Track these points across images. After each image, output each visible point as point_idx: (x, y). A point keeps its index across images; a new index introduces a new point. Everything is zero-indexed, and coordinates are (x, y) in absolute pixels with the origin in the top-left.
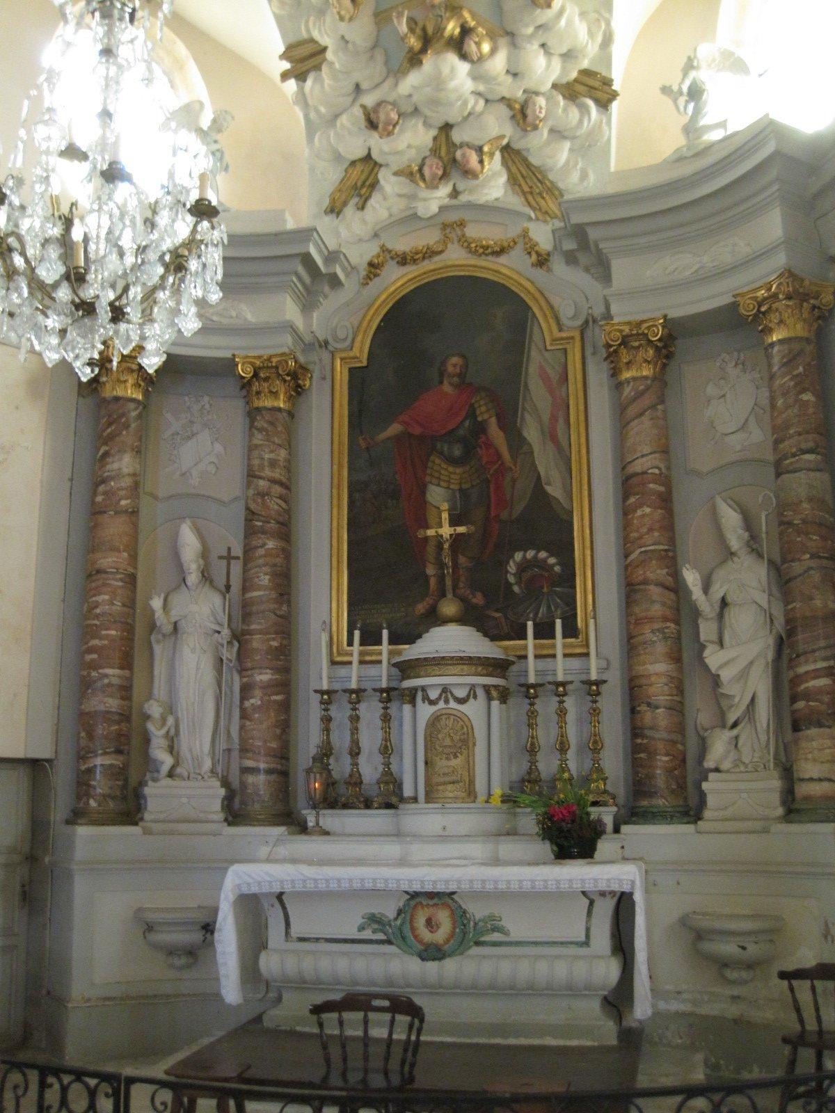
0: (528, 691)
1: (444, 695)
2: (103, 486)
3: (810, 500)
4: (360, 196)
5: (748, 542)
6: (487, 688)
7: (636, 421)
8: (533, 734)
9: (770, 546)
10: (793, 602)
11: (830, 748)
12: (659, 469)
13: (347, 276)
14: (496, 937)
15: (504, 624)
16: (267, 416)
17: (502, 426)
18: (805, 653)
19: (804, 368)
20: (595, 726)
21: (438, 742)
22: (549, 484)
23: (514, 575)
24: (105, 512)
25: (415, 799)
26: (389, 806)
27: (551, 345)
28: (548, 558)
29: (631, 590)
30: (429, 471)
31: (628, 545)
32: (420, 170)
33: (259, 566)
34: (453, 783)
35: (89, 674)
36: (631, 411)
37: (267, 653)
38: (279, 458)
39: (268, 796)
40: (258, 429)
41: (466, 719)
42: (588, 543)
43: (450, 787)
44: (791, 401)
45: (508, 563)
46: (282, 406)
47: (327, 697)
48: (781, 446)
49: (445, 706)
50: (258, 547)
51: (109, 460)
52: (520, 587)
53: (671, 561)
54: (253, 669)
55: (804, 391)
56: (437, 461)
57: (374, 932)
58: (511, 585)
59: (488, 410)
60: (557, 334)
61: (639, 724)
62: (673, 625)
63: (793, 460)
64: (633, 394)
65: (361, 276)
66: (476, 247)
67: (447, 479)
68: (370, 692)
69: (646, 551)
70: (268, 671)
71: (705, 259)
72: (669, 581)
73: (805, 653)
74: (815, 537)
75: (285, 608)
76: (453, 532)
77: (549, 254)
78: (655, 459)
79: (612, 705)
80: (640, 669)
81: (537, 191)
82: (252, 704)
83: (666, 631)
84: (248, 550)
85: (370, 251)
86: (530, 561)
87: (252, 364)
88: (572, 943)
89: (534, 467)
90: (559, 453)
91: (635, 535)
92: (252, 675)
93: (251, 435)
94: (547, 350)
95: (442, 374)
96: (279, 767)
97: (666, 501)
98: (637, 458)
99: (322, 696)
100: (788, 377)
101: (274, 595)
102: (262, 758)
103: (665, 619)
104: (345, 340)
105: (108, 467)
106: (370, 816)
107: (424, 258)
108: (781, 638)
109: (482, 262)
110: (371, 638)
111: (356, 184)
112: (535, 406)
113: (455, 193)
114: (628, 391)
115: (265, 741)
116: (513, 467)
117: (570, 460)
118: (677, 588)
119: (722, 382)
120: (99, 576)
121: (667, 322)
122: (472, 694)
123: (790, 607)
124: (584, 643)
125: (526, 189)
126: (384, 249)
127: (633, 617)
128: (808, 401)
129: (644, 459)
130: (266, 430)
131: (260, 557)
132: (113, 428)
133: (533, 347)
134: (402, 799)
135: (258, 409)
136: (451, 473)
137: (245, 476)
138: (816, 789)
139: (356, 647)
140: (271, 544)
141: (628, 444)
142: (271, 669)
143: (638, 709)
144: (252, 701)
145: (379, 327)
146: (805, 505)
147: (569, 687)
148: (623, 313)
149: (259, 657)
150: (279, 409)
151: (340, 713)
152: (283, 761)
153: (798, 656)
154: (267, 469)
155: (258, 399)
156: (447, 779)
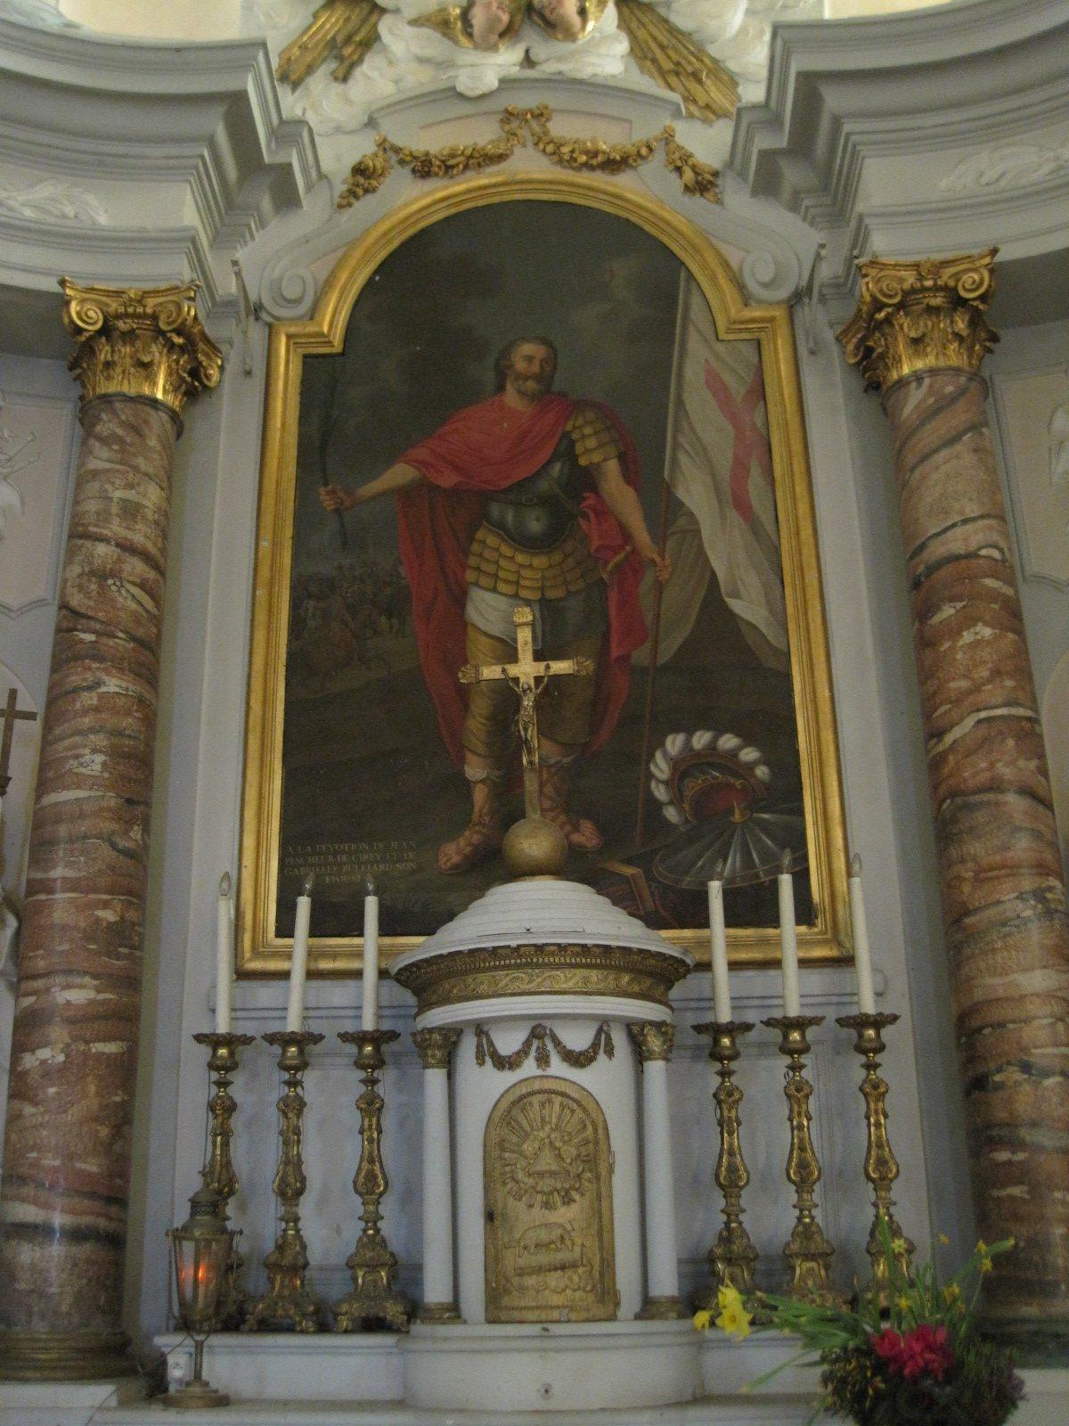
0: (716, 1042)
1: (535, 1043)
4: (341, 59)
6: (636, 1032)
7: (944, 453)
8: (731, 1145)
12: (1001, 551)
13: (309, 188)
15: (646, 893)
16: (126, 412)
17: (631, 475)
21: (522, 1163)
25: (453, 1311)
26: (372, 1325)
27: (729, 330)
30: (472, 561)
32: (465, 16)
33: (79, 732)
34: (563, 1268)
37: (89, 938)
38: (145, 502)
39: (69, 1299)
41: (591, 1106)
42: (826, 717)
43: (554, 1279)
45: (651, 756)
46: (160, 396)
49: (539, 1072)
50: (84, 689)
52: (681, 810)
54: (47, 974)
56: (492, 540)
59: (600, 446)
60: (735, 311)
64: (931, 401)
65: (337, 193)
66: (573, 151)
67: (512, 577)
68: (331, 1041)
70: (87, 980)
75: (136, 833)
76: (542, 673)
77: (716, 174)
78: (991, 528)
80: (990, 984)
81: (690, 69)
82: (43, 1062)
83: (1049, 895)
84: (58, 700)
85: (362, 148)
86: (698, 754)
87: (102, 306)
89: (701, 553)
92: (47, 990)
93: (85, 451)
95: (502, 375)
96: (102, 1223)
98: (954, 525)
99: (215, 1051)
101: (111, 800)
102: (59, 1201)
104: (297, 302)
106: (334, 1352)
107: (466, 167)
109: (585, 178)
111: (334, 38)
112: (699, 439)
113: (528, 61)
114: (914, 400)
115: (71, 1157)
116: (658, 559)
117: (777, 550)
122: (601, 1045)
124: (829, 936)
125: (667, 65)
126: (384, 146)
127: (970, 865)
129: (969, 527)
131: (86, 711)
133: (691, 329)
134: (415, 1310)
135: (107, 399)
136: (521, 566)
137: (65, 537)
139: (301, 939)
140: (112, 685)
142: (95, 976)
143: (997, 1078)
144: (44, 1053)
145: (370, 283)
149: (65, 947)
150: (154, 403)
152: (114, 1210)
154: (116, 521)
155: (109, 378)
156: (544, 1258)
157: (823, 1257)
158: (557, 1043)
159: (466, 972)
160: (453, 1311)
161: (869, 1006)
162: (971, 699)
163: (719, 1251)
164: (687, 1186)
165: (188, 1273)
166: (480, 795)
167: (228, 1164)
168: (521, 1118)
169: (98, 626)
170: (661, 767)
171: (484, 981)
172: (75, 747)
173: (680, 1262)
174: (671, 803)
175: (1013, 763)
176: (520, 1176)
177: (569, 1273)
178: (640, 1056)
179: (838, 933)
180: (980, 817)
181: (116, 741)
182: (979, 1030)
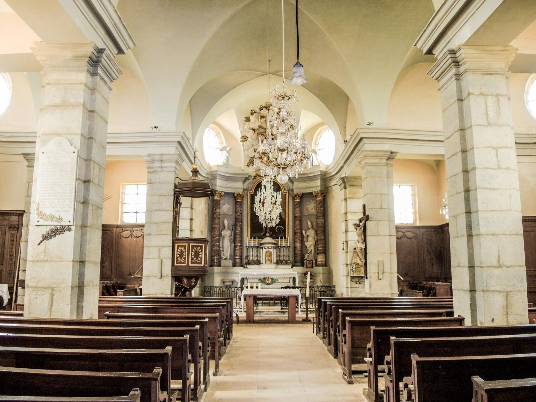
3: (321, 223)
6: (274, 247)
14: (277, 282)
25: (263, 263)
29: (295, 234)
36: (296, 206)
47: (248, 248)
53: (301, 229)
71: (309, 184)
72: (301, 232)
79: (291, 250)
97: (300, 220)
110: (255, 238)
114: (296, 203)
118: (302, 233)
122: (272, 248)
139: (253, 240)
148: (296, 191)
160: (263, 263)
161: (289, 245)
164: (277, 256)
166: (264, 230)
170: (276, 228)
178: (274, 248)
179: (287, 240)
181: (182, 162)
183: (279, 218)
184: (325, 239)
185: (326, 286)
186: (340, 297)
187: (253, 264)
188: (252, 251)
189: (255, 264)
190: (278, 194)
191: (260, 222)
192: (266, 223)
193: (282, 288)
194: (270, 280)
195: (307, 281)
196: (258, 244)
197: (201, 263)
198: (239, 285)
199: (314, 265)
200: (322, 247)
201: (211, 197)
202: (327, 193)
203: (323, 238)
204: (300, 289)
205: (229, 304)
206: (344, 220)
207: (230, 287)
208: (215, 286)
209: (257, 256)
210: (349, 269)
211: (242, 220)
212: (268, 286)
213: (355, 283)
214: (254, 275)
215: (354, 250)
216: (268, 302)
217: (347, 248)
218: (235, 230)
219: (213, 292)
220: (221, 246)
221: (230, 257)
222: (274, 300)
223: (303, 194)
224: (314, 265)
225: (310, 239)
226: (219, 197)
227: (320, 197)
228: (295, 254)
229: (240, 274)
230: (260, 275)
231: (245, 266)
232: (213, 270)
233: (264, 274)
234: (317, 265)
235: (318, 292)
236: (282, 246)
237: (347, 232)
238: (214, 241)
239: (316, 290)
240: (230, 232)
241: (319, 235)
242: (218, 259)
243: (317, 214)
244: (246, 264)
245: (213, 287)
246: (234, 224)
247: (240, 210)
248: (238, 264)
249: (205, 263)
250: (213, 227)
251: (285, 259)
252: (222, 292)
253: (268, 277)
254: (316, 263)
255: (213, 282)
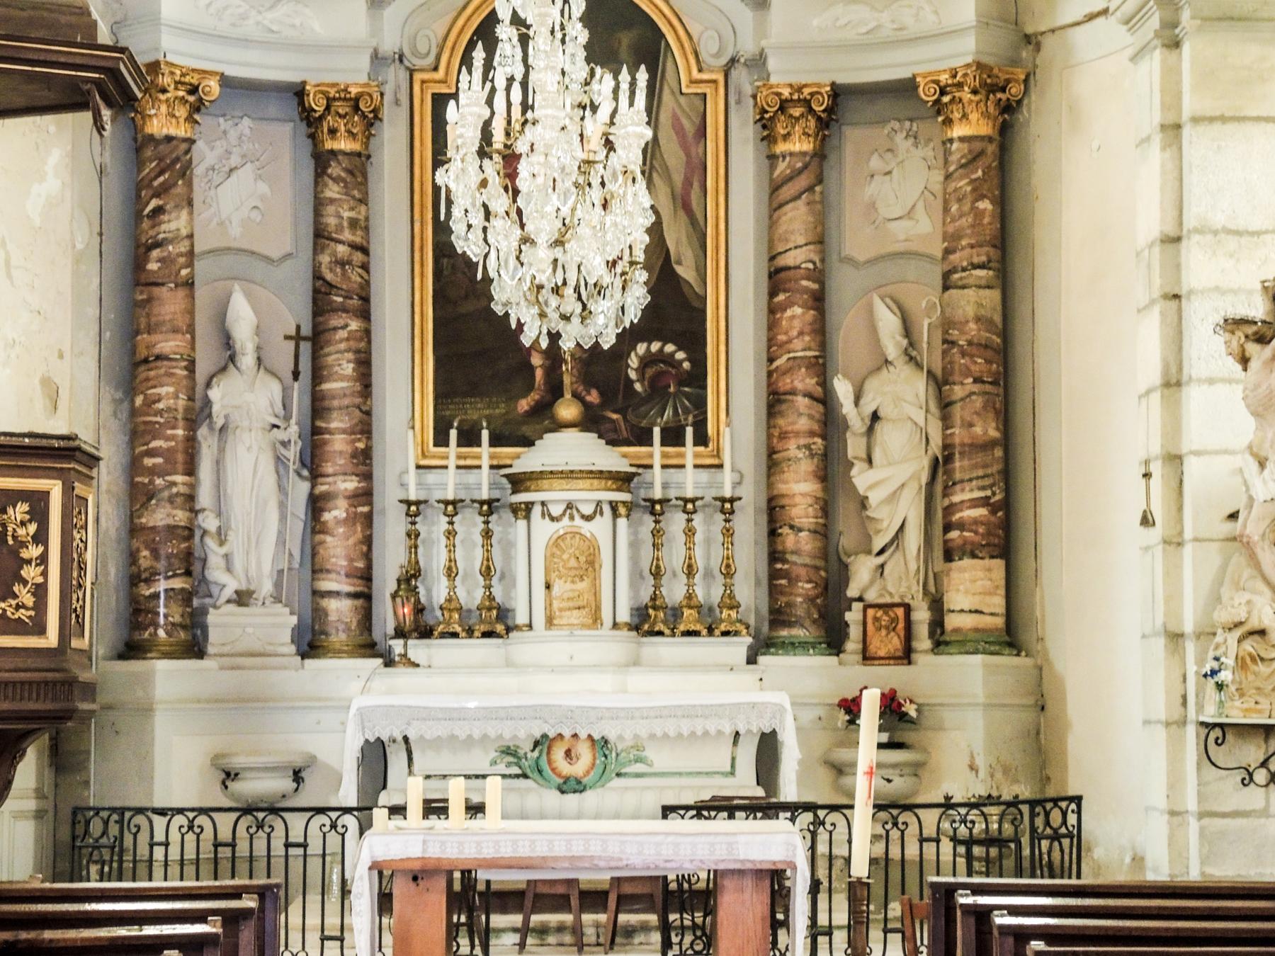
0: (653, 507)
1: (569, 511)
2: (158, 250)
3: (978, 319)
5: (906, 349)
6: (614, 506)
7: (790, 206)
9: (932, 356)
10: (952, 427)
11: (982, 579)
12: (814, 263)
14: (639, 768)
18: (962, 481)
19: (983, 171)
20: (728, 549)
22: (679, 263)
23: (636, 370)
24: (163, 284)
28: (676, 352)
29: (775, 401)
31: (774, 348)
34: (579, 608)
35: (152, 482)
36: (787, 192)
40: (334, 179)
44: (966, 208)
45: (629, 355)
47: (414, 508)
48: (952, 257)
51: (165, 217)
52: (643, 385)
53: (822, 367)
55: (982, 197)
57: (509, 765)
58: (632, 382)
60: (696, 75)
61: (780, 548)
62: (819, 441)
63: (964, 274)
64: (788, 171)
69: (794, 358)
70: (354, 478)
71: (885, 17)
73: (962, 481)
74: (979, 360)
79: (748, 525)
80: (782, 488)
82: (335, 517)
86: (654, 355)
88: (718, 773)
90: (692, 224)
91: (782, 338)
92: (335, 482)
94: (681, 93)
97: (819, 301)
98: (790, 249)
100: (967, 180)
103: (812, 434)
105: (164, 227)
108: (937, 459)
110: (469, 438)
114: (782, 167)
117: (705, 235)
118: (826, 400)
119: (889, 155)
120: (159, 363)
121: (833, 84)
122: (598, 510)
123: (949, 432)
124: (715, 453)
128: (985, 209)
129: (798, 250)
130: (344, 180)
131: (341, 341)
132: (167, 176)
138: (967, 622)
141: (780, 231)
143: (780, 531)
144: (335, 513)
146: (972, 325)
147: (698, 503)
151: (434, 526)
153: (954, 484)
157: (699, 607)
158: (578, 510)
159: (537, 479)
160: (530, 626)
162: (787, 346)
163: (650, 604)
164: (636, 576)
165: (400, 612)
166: (539, 373)
167: (417, 562)
168: (562, 544)
169: (343, 293)
170: (634, 362)
171: (545, 483)
172: (339, 359)
173: (632, 609)
174: (638, 380)
175: (803, 380)
176: (561, 569)
177: (582, 610)
178: (615, 514)
180: (784, 407)
181: (358, 356)
182: (775, 508)
183: (642, 276)
184: (1007, 440)
185: (1007, 797)
186: (1121, 876)
187: (455, 635)
188: (451, 534)
189: (470, 633)
190: (625, 86)
191: (499, 310)
192: (542, 315)
193: (667, 811)
194: (585, 754)
195: (853, 765)
196: (493, 486)
197: (41, 630)
198: (348, 795)
199: (923, 642)
200: (985, 502)
201: (106, 114)
202: (1026, 81)
203: (994, 433)
204: (807, 817)
205: (247, 935)
206: (1156, 294)
207: (274, 811)
208: (158, 803)
209: (487, 572)
210: (1192, 669)
211: (366, 299)
212: (571, 798)
213: (1239, 775)
214: (458, 715)
215: (1228, 528)
216: (568, 918)
217: (1180, 509)
218: (318, 376)
219: (143, 851)
220: (205, 498)
221: (278, 585)
222: (528, 903)
223: (837, 92)
224: (923, 642)
225: (893, 439)
226: (182, 112)
227: (974, 116)
228: (775, 556)
229: (353, 711)
230: (506, 714)
231: (397, 646)
232: (146, 680)
233: (537, 712)
234: (941, 640)
235: (946, 846)
236: (672, 494)
237: (1179, 384)
238: (149, 462)
239: (930, 831)
240: (275, 388)
241: (957, 411)
242: (186, 597)
243: (947, 252)
244: (400, 633)
245: (140, 811)
246: (306, 330)
247: (354, 223)
248: (338, 637)
249: (71, 620)
250: (142, 353)
251: (700, 593)
252: (206, 846)
253: (567, 733)
254: (937, 624)
255: (147, 777)
